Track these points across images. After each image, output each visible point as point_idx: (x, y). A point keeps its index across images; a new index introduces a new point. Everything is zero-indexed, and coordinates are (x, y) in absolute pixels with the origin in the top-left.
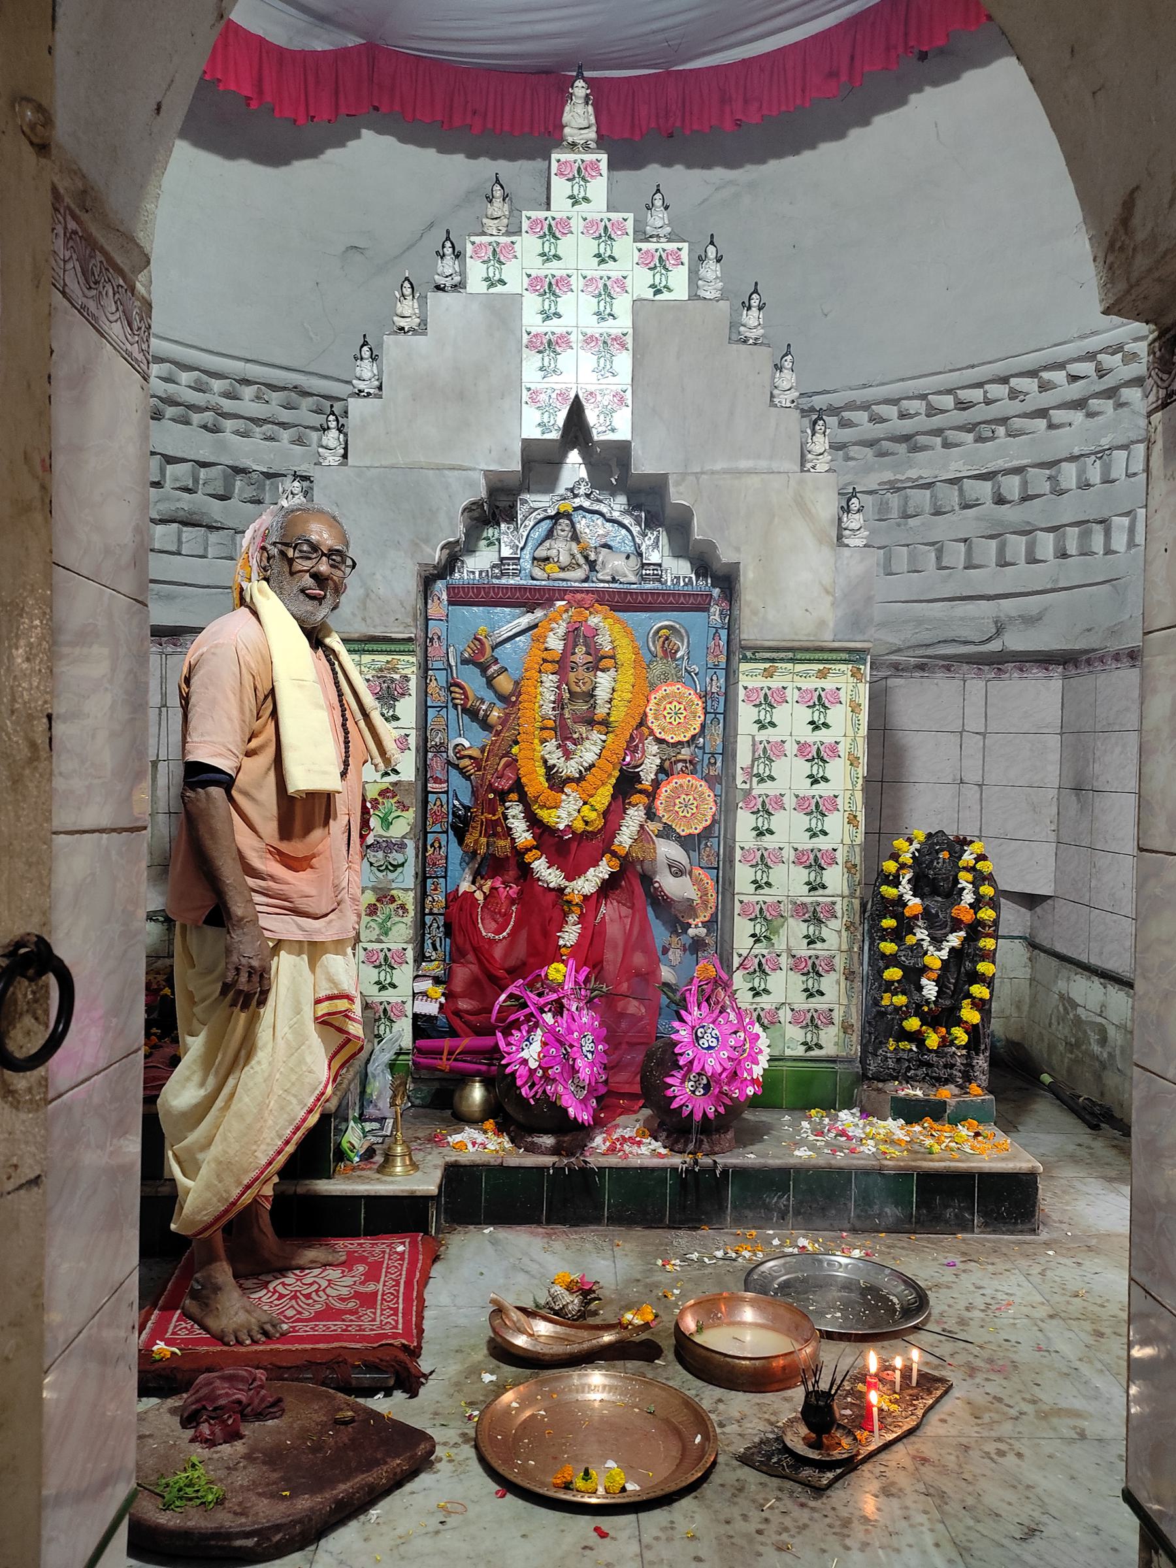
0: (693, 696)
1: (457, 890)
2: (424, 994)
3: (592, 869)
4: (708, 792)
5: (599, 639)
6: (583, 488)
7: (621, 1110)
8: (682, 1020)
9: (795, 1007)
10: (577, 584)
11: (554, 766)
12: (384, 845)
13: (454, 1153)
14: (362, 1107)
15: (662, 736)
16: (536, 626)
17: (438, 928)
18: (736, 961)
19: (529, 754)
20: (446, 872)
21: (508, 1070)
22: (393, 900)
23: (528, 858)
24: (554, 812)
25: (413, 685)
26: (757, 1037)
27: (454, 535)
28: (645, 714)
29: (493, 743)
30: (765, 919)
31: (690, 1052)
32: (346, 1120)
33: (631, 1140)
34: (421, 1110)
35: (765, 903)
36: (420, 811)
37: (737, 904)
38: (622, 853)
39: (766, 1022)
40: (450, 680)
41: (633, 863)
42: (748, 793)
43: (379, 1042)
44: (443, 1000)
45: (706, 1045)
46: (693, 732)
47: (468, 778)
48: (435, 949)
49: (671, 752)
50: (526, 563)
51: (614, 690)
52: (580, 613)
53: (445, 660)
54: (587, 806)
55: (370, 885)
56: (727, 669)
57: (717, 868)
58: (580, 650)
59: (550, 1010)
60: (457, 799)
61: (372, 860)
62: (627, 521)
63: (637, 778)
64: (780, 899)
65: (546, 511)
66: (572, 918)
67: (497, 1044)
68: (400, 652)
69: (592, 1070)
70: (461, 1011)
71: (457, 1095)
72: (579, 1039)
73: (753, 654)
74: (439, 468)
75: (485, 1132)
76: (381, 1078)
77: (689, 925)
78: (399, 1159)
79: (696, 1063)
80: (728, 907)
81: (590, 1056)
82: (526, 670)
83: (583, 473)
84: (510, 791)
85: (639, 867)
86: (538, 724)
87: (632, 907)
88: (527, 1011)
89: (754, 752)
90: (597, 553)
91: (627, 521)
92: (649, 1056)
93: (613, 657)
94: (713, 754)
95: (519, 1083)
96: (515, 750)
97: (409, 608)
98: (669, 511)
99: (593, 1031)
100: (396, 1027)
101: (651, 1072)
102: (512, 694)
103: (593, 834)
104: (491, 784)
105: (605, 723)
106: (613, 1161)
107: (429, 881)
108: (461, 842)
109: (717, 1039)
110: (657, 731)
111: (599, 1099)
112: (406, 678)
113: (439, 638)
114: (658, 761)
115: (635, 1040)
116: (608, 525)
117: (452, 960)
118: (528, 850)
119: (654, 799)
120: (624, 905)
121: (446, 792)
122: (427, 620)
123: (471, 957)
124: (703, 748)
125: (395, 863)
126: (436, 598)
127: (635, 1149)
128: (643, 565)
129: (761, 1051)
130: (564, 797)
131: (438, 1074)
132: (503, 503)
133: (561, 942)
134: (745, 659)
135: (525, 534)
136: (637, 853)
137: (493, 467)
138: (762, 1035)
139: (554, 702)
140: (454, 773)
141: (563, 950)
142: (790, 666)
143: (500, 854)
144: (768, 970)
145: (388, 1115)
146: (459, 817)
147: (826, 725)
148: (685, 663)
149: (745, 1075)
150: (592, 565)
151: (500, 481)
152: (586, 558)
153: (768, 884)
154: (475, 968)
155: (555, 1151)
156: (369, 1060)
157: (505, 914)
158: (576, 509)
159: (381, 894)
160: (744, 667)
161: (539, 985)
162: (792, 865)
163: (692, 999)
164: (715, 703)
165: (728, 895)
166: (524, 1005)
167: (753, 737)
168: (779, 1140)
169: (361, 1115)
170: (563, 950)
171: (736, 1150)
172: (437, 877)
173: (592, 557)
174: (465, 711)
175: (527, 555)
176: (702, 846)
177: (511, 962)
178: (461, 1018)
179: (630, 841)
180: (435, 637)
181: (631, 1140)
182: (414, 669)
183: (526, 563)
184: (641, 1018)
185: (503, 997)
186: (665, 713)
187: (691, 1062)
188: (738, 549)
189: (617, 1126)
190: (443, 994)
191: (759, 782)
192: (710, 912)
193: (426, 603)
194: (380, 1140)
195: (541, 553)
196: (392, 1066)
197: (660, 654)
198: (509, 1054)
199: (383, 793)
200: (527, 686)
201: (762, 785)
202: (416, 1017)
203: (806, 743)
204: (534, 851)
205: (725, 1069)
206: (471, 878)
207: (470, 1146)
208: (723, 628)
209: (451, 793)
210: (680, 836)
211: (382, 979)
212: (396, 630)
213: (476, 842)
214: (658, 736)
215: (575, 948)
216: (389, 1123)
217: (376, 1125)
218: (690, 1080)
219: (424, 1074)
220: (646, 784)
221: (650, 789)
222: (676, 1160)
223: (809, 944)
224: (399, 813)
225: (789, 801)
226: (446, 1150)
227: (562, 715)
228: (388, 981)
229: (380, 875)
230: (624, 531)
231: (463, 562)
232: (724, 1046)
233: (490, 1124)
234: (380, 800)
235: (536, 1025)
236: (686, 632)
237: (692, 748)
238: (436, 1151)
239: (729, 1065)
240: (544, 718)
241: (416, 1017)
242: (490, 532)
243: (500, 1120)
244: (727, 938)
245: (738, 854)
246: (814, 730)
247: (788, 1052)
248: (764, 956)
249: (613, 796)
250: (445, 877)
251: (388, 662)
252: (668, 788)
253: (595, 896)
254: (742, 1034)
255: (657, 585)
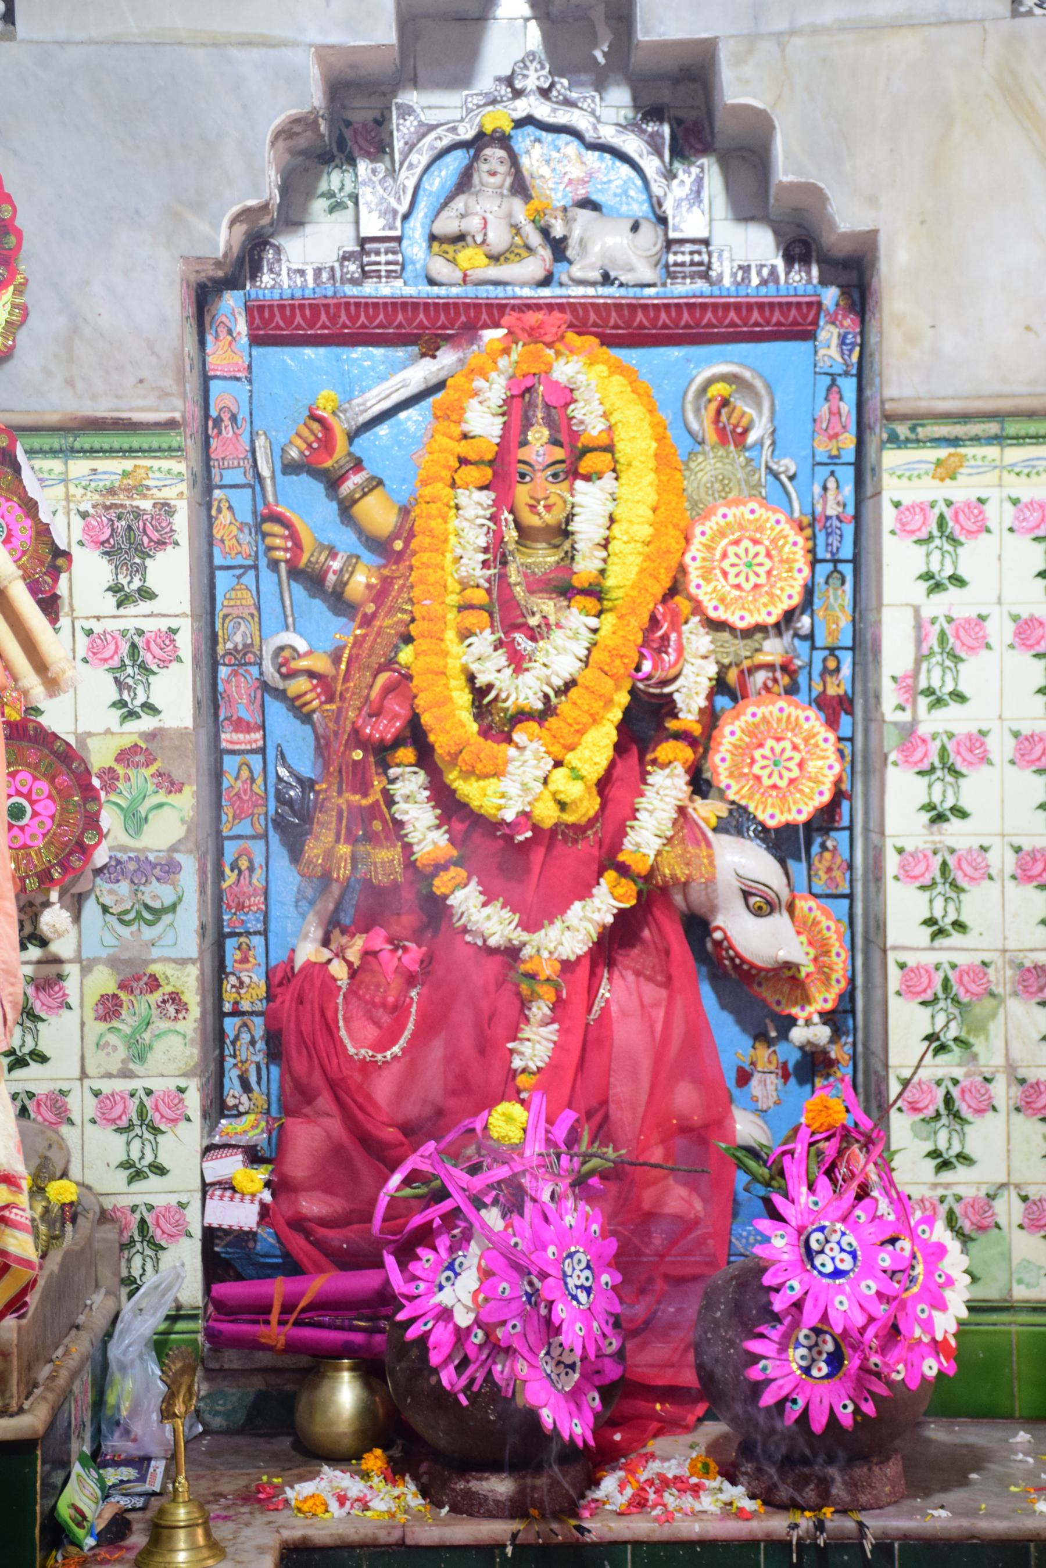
0: (786, 528)
1: (291, 960)
2: (228, 1186)
3: (577, 905)
4: (823, 732)
5: (577, 411)
6: (532, 74)
7: (654, 1425)
8: (775, 1215)
10: (526, 292)
11: (490, 687)
12: (132, 866)
13: (299, 1520)
14: (98, 1435)
15: (721, 615)
16: (440, 386)
17: (253, 1042)
19: (434, 662)
20: (266, 922)
22: (154, 984)
23: (440, 885)
24: (492, 785)
25: (181, 522)
26: (941, 1250)
28: (682, 569)
29: (358, 642)
30: (956, 1001)
32: (65, 1465)
33: (679, 1483)
34: (223, 1440)
35: (954, 966)
36: (206, 793)
37: (894, 973)
38: (641, 867)
39: (967, 1227)
40: (260, 507)
41: (664, 890)
42: (909, 731)
43: (131, 1295)
44: (267, 1196)
45: (829, 1269)
46: (786, 605)
47: (306, 718)
48: (246, 1087)
49: (742, 648)
50: (416, 248)
51: (612, 520)
52: (537, 357)
53: (248, 464)
54: (561, 772)
55: (104, 954)
56: (859, 465)
57: (850, 896)
58: (538, 435)
59: (495, 1202)
60: (285, 764)
61: (107, 900)
62: (632, 145)
63: (667, 707)
64: (987, 957)
65: (454, 130)
66: (540, 1010)
67: (387, 1283)
69: (589, 1328)
70: (310, 1220)
72: (559, 1261)
73: (913, 429)
74: (217, 44)
75: (365, 1476)
76: (137, 1371)
77: (792, 1021)
78: (182, 1534)
79: (808, 1306)
80: (878, 979)
81: (582, 1296)
82: (424, 483)
83: (534, 37)
84: (398, 742)
85: (678, 899)
86: (453, 599)
87: (668, 983)
88: (446, 1206)
89: (919, 642)
90: (568, 221)
91: (632, 145)
93: (609, 448)
94: (832, 650)
96: (406, 655)
99: (588, 1243)
103: (579, 830)
104: (356, 731)
105: (595, 592)
107: (230, 944)
108: (296, 854)
109: (853, 1254)
110: (708, 605)
111: (606, 1393)
112: (166, 508)
113: (234, 418)
114: (712, 670)
116: (592, 156)
117: (287, 1110)
118: (441, 867)
119: (706, 751)
120: (650, 979)
122: (206, 379)
123: (324, 1101)
124: (811, 637)
125: (157, 905)
127: (688, 1501)
128: (669, 244)
129: (950, 1282)
130: (512, 751)
131: (263, 1358)
132: (361, 114)
133: (517, 1063)
134: (894, 439)
135: (411, 184)
136: (672, 868)
137: (336, 38)
138: (953, 1245)
139: (486, 550)
140: (276, 709)
141: (522, 1080)
142: (992, 452)
143: (380, 878)
144: (966, 1113)
145: (154, 1449)
146: (290, 803)
147: (957, 580)
148: (766, 452)
149: (918, 1332)
150: (558, 248)
151: (352, 66)
152: (545, 232)
154: (335, 1125)
156: (109, 1335)
157: (395, 1008)
158: (520, 124)
159: (128, 972)
160: (892, 458)
161: (471, 1151)
162: (1010, 884)
164: (834, 540)
165: (876, 955)
166: (442, 1194)
167: (917, 610)
168: (1004, 1481)
169: (96, 1453)
171: (907, 1503)
172: (248, 934)
173: (558, 231)
174: (296, 573)
175: (416, 230)
176: (815, 849)
177: (411, 1110)
178: (307, 1233)
179: (656, 844)
180: (226, 417)
181: (679, 1483)
182: (183, 487)
183: (416, 248)
184: (696, 1223)
185: (396, 1179)
186: (726, 565)
187: (798, 1305)
188: (873, 201)
189: (652, 1456)
190: (268, 1184)
192: (836, 990)
193: (202, 343)
194: (139, 1502)
195: (447, 225)
196: (160, 1346)
197: (711, 436)
198: (411, 1298)
199: (124, 756)
200: (423, 518)
201: (939, 713)
202: (210, 1235)
203: (1032, 619)
204: (454, 871)
205: (871, 1319)
207: (334, 1506)
208: (846, 374)
209: (271, 753)
210: (765, 829)
211: (135, 1155)
212: (140, 403)
213: (329, 854)
214: (713, 614)
215: (548, 1074)
217: (128, 1473)
218: (798, 1345)
220: (688, 717)
221: (697, 730)
222: (777, 1524)
224: (161, 797)
225: (1001, 747)
226: (281, 1517)
227: (503, 577)
228: (149, 1158)
229: (125, 931)
230: (625, 169)
231: (278, 250)
232: (869, 1270)
233: (374, 1460)
234: (120, 770)
235: (467, 1237)
236: (768, 387)
237: (788, 636)
238: (260, 1519)
240: (464, 585)
241: (210, 1235)
242: (334, 179)
243: (396, 1453)
244: (876, 1046)
245: (892, 863)
248: (955, 1082)
249: (619, 748)
250: (265, 933)
251: (125, 474)
252: (738, 726)
253: (586, 963)
254: (905, 1245)
255: (700, 286)
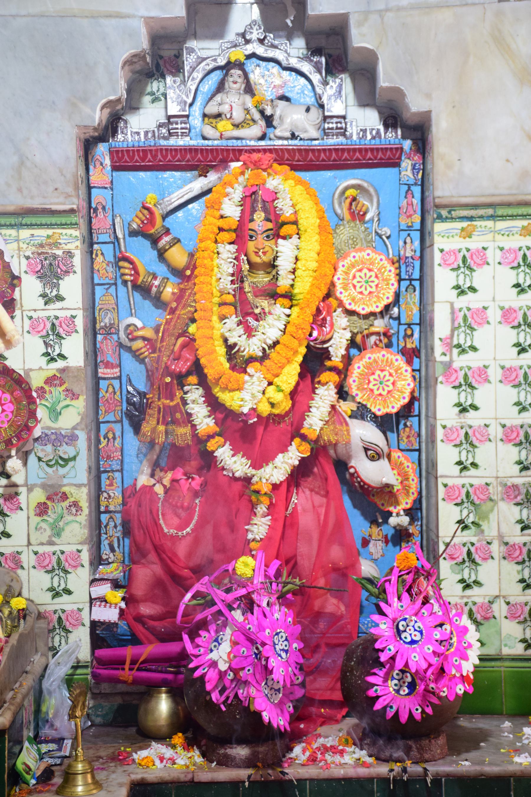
0: (385, 263)
1: (135, 485)
2: (103, 600)
3: (280, 456)
5: (279, 204)
6: (255, 32)
7: (322, 720)
8: (381, 613)
9: (512, 600)
10: (253, 143)
11: (235, 345)
12: (53, 437)
13: (140, 770)
14: (37, 728)
15: (353, 307)
17: (115, 527)
18: (442, 548)
19: (207, 332)
21: (197, 674)
22: (65, 497)
23: (211, 445)
24: (237, 395)
25: (77, 261)
26: (465, 630)
27: (114, 91)
28: (333, 284)
29: (168, 322)
30: (473, 503)
31: (391, 647)
32: (20, 743)
33: (333, 749)
35: (471, 486)
36: (91, 399)
38: (313, 436)
40: (118, 253)
42: (448, 366)
43: (54, 656)
44: (123, 605)
45: (409, 640)
46: (386, 302)
47: (142, 361)
48: (112, 550)
49: (363, 324)
50: (196, 121)
51: (297, 259)
52: (258, 176)
53: (111, 232)
54: (272, 388)
55: (39, 482)
57: (419, 450)
58: (259, 216)
60: (131, 385)
61: (41, 454)
62: (306, 68)
63: (326, 354)
64: (488, 481)
65: (215, 60)
66: (262, 509)
67: (184, 649)
68: (62, 225)
69: (287, 671)
70: (143, 616)
71: (141, 712)
73: (449, 212)
75: (174, 747)
76: (57, 695)
77: (390, 514)
78: (80, 777)
79: (398, 659)
81: (284, 655)
82: (201, 241)
84: (189, 373)
85: (332, 452)
87: (327, 495)
88: (214, 609)
89: (453, 321)
90: (273, 107)
91: (306, 68)
92: (349, 657)
93: (295, 223)
94: (409, 325)
95: (209, 687)
96: (192, 329)
97: (69, 176)
98: (352, 56)
99: (286, 628)
100: (72, 637)
101: (351, 672)
102: (187, 268)
103: (280, 417)
104: (167, 367)
105: (289, 296)
106: (312, 772)
107: (104, 476)
109: (421, 632)
110: (346, 302)
112: (69, 254)
113: (104, 208)
114: (348, 335)
115: (335, 641)
116: (286, 74)
117: (133, 561)
118: (211, 437)
119: (346, 377)
120: (317, 493)
121: (120, 378)
122: (89, 188)
123: (152, 556)
124: (398, 318)
125: (66, 457)
126: (98, 164)
127: (338, 758)
128: (325, 118)
129: (470, 646)
130: (247, 378)
131: (121, 688)
132: (168, 52)
133: (250, 536)
134: (440, 217)
135: (193, 88)
136: (329, 436)
137: (155, 13)
138: (472, 627)
139: (233, 275)
140: (126, 357)
141: (253, 545)
142: (490, 224)
143: (180, 443)
144: (478, 560)
145: (66, 734)
146: (134, 404)
147: (473, 289)
148: (375, 224)
149: (454, 671)
150: (269, 120)
151: (162, 28)
152: (262, 112)
153: (474, 465)
154: (158, 569)
155: (249, 763)
157: (188, 508)
158: (249, 57)
159: (51, 491)
160: (439, 227)
161: (226, 581)
162: (500, 444)
163: (391, 589)
164: (410, 269)
165: (432, 480)
167: (452, 304)
170: (253, 545)
171: (449, 758)
172: (113, 471)
173: (268, 112)
174: (136, 287)
175: (196, 111)
176: (401, 426)
177: (196, 561)
178: (143, 624)
179: (320, 424)
180: (100, 207)
181: (333, 749)
182: (78, 243)
183: (196, 121)
184: (341, 617)
186: (355, 282)
187: (393, 658)
188: (428, 96)
189: (320, 736)
190: (123, 599)
191: (460, 353)
192: (412, 498)
193: (87, 169)
194: (58, 761)
195: (212, 109)
196: (69, 682)
197: (347, 216)
198: (196, 656)
199: (49, 381)
200: (201, 259)
201: (463, 357)
202: (94, 625)
203: (511, 308)
204: (217, 438)
205: (430, 665)
206: (149, 471)
207: (157, 762)
208: (416, 184)
210: (376, 416)
211: (56, 585)
212: (56, 200)
213: (154, 430)
214: (348, 307)
215: (266, 541)
216: (68, 743)
217: (52, 746)
218: (393, 678)
219: (105, 687)
220: (336, 358)
221: (341, 366)
223: (522, 529)
224: (68, 402)
225: (495, 374)
227: (241, 289)
228: (63, 586)
229: (49, 470)
230: (303, 80)
231: (126, 122)
232: (429, 640)
233: (178, 739)
234: (47, 388)
236: (376, 191)
237: (387, 318)
238: (120, 769)
239: (435, 660)
240: (222, 293)
241: (94, 625)
242: (154, 86)
243: (189, 735)
244: (432, 526)
245: (440, 433)
246: (519, 293)
247: (506, 651)
248: (473, 544)
249: (301, 376)
250: (121, 471)
251: (48, 237)
252: (361, 364)
253: (285, 485)
255: (341, 140)
